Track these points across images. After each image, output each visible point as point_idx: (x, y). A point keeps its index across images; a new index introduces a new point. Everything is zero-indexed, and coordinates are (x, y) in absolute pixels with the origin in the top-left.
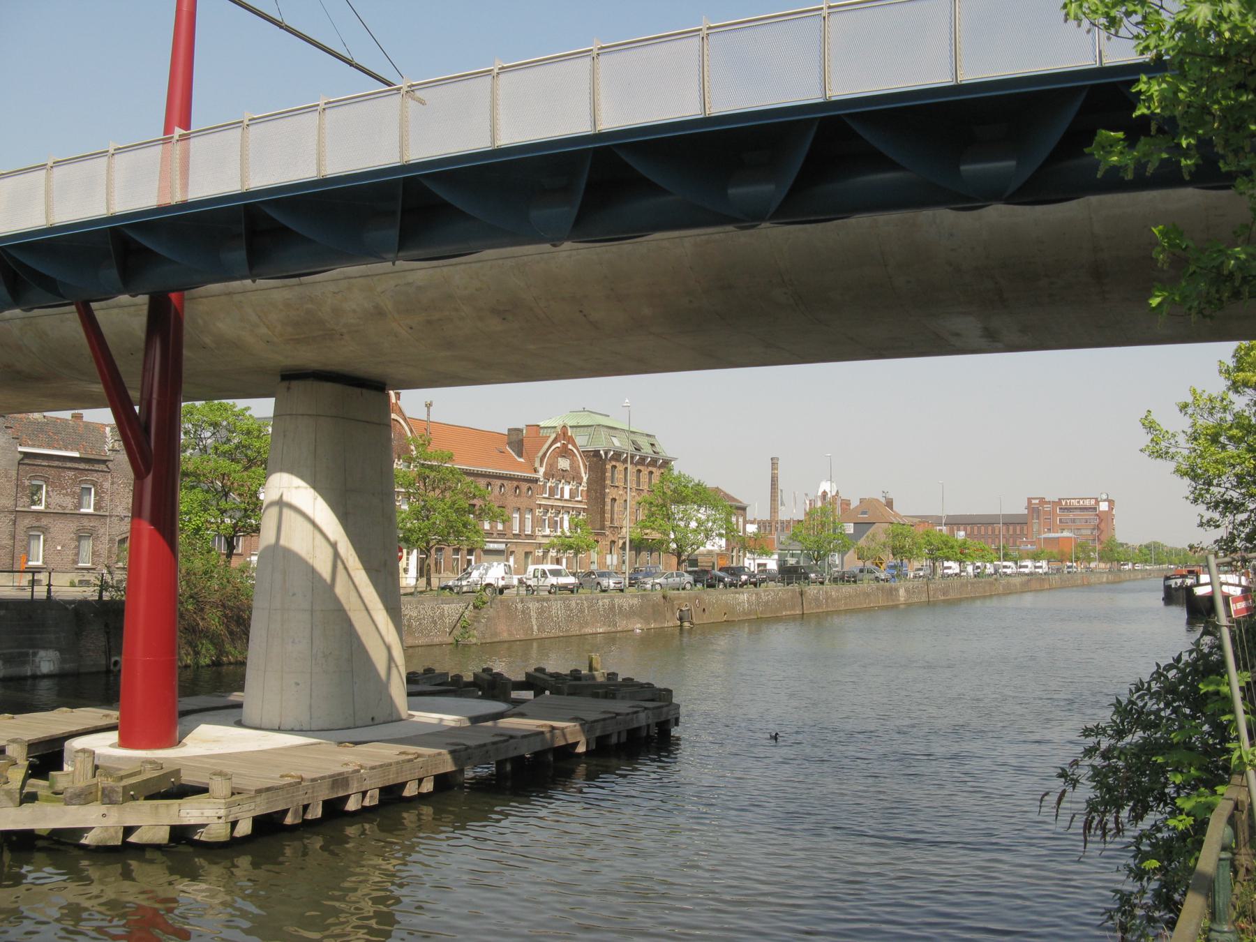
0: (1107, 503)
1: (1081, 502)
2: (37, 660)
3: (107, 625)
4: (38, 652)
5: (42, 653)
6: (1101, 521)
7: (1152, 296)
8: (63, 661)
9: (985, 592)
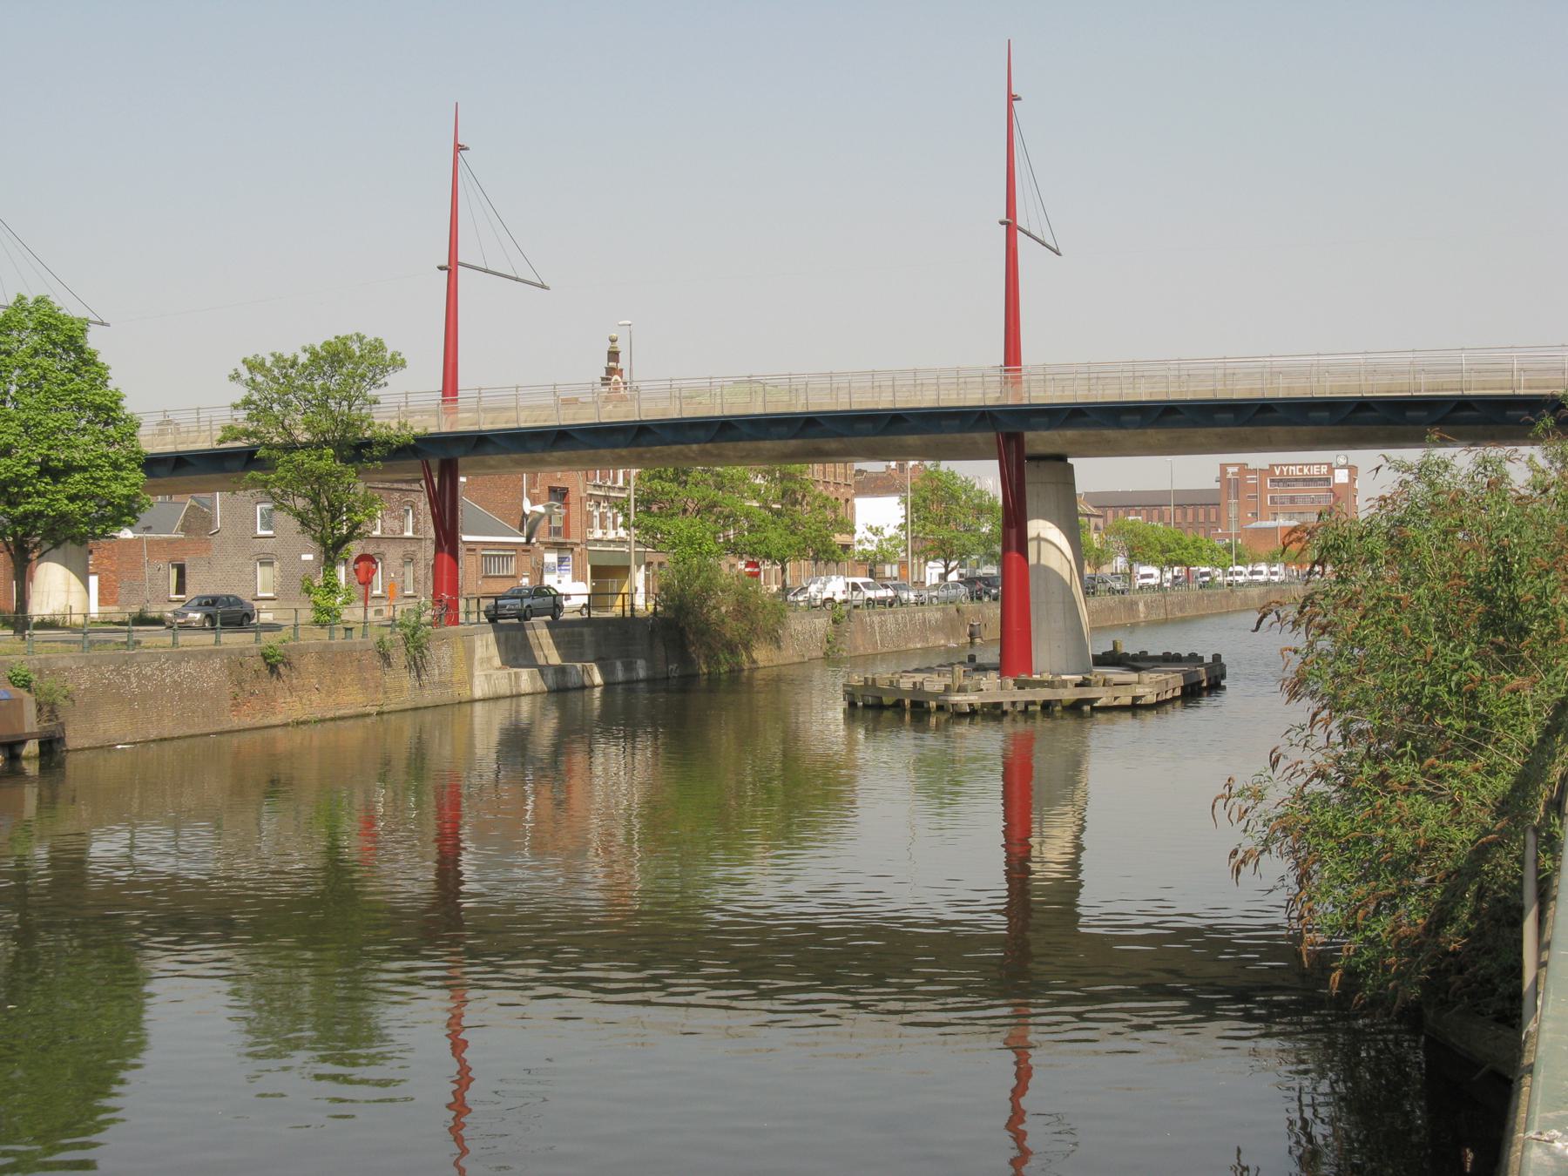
0: (1346, 471)
1: (1306, 471)
6: (1337, 499)
9: (1222, 608)
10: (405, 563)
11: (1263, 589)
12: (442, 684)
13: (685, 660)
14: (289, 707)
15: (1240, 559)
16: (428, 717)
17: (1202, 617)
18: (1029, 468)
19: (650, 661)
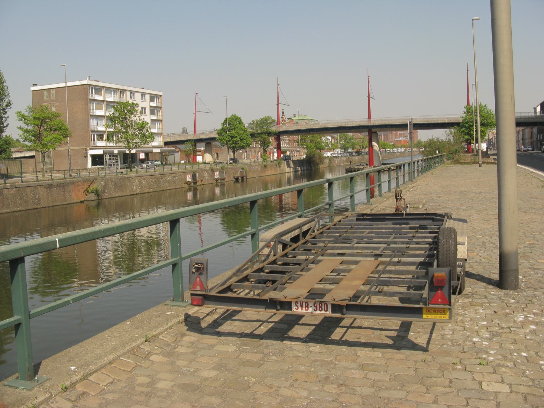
10: (254, 152)
11: (400, 153)
12: (282, 170)
13: (311, 167)
14: (268, 173)
15: (395, 147)
16: (281, 175)
17: (389, 159)
18: (372, 134)
19: (306, 166)
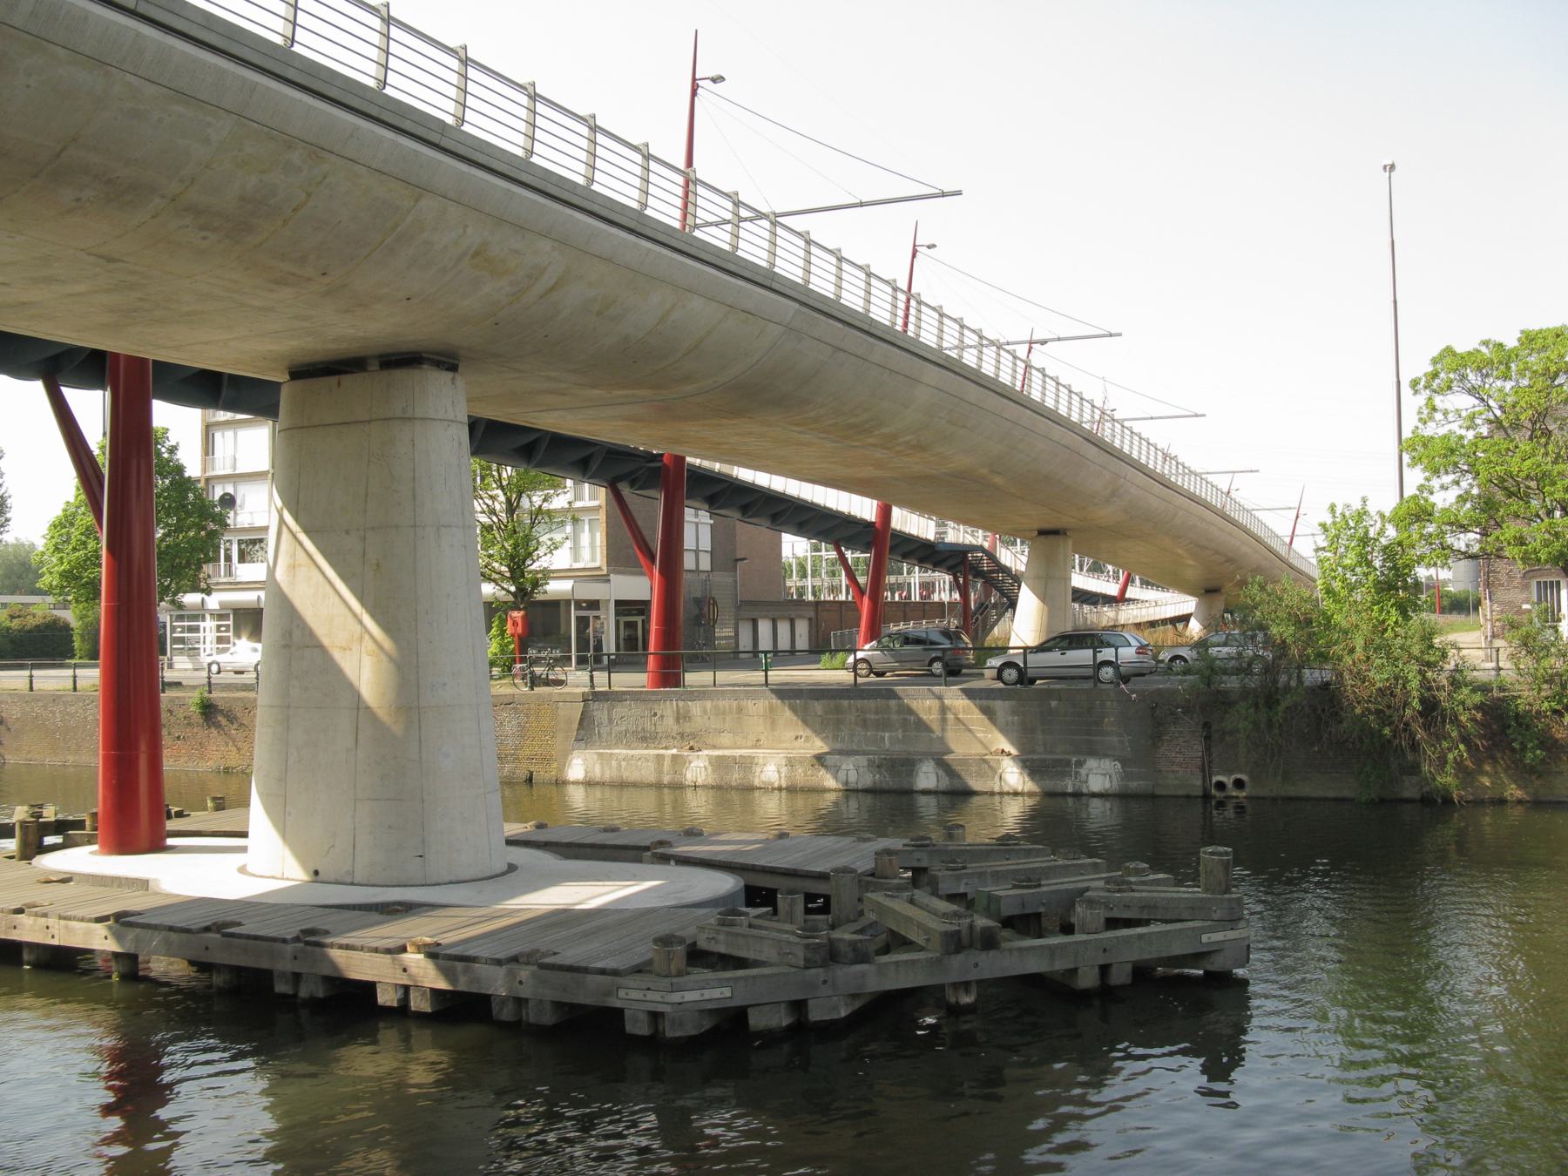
2: (1083, 771)
3: (1207, 725)
4: (1085, 761)
5: (1092, 763)
7: (929, 1015)
8: (1126, 776)
